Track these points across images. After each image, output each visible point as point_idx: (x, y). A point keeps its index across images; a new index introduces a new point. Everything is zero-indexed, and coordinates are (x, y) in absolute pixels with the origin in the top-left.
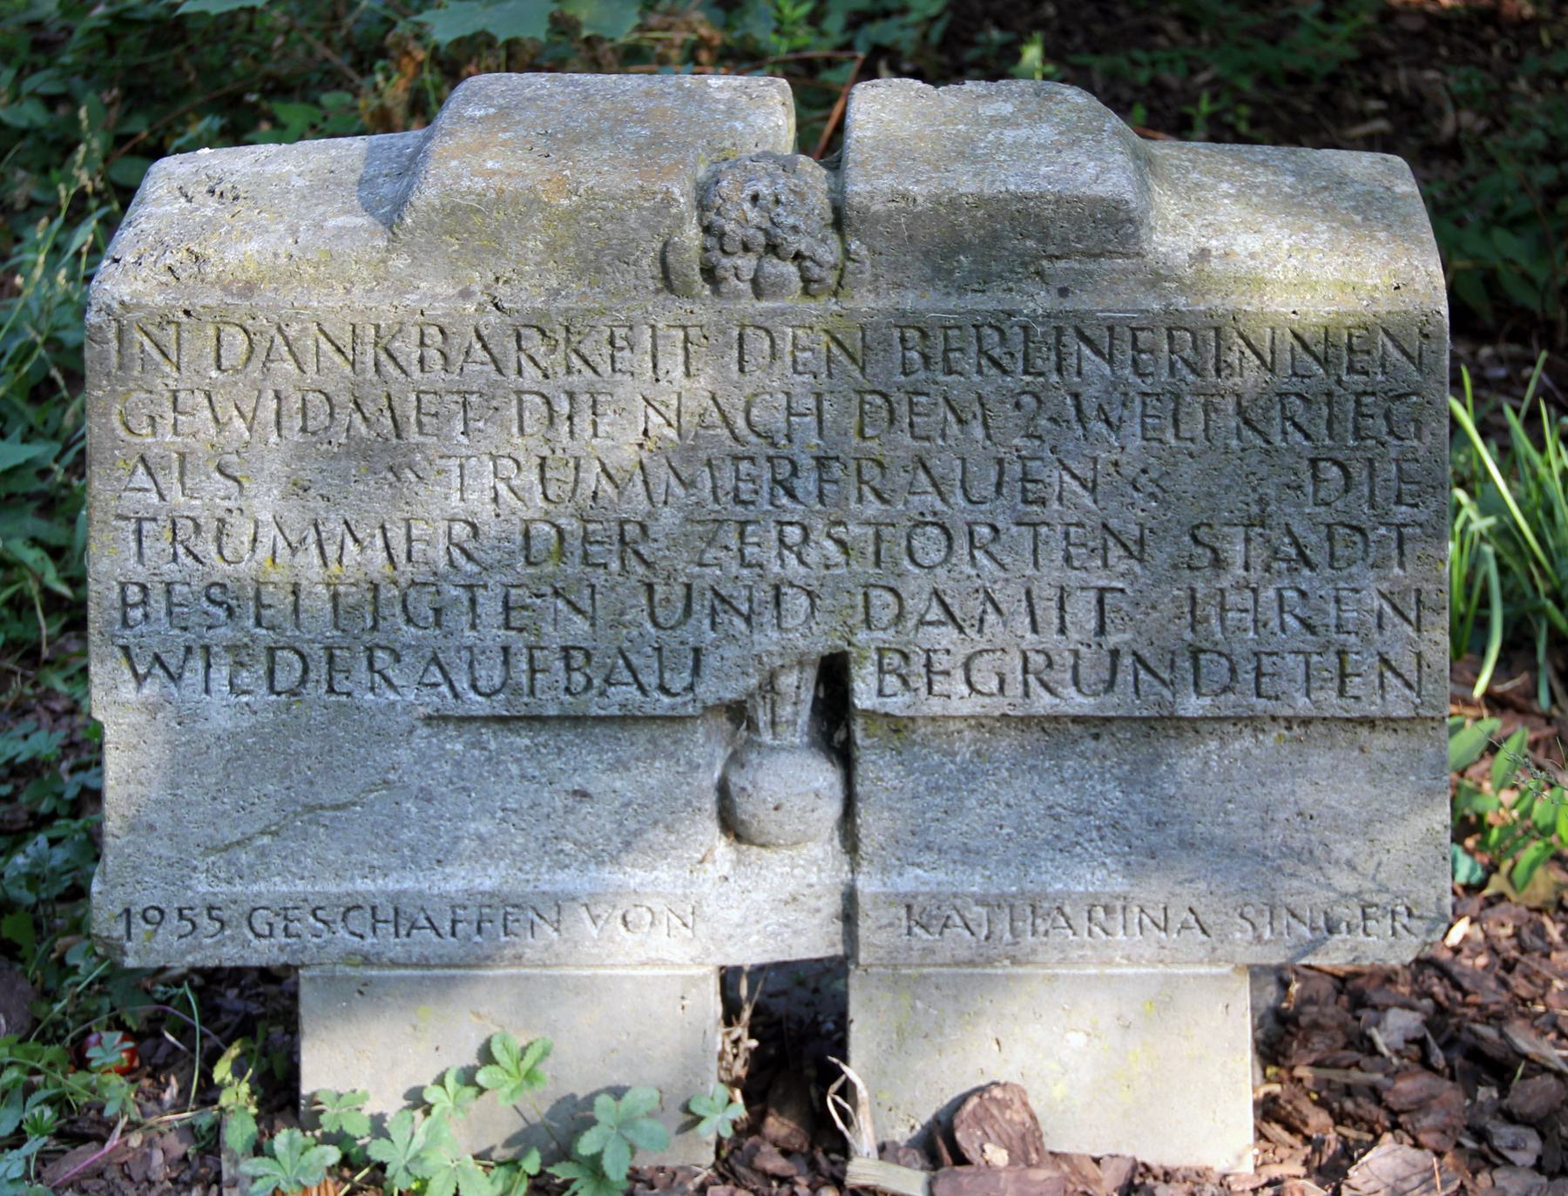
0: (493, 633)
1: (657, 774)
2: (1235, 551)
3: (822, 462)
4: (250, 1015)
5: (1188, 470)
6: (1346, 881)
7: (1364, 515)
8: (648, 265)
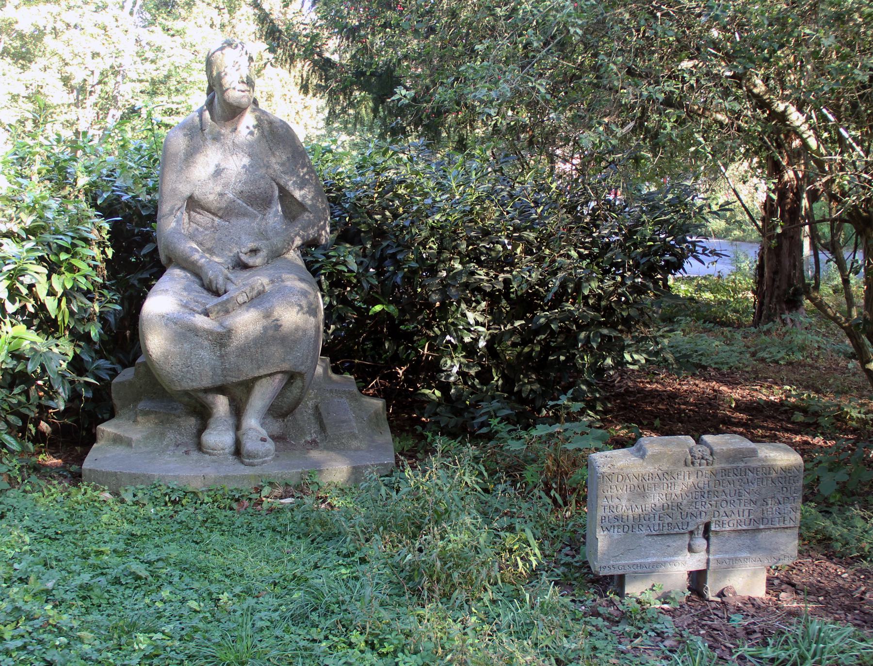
0: (657, 521)
1: (679, 543)
2: (770, 502)
4: (618, 582)
5: (764, 490)
6: (782, 553)
7: (789, 495)
8: (683, 463)
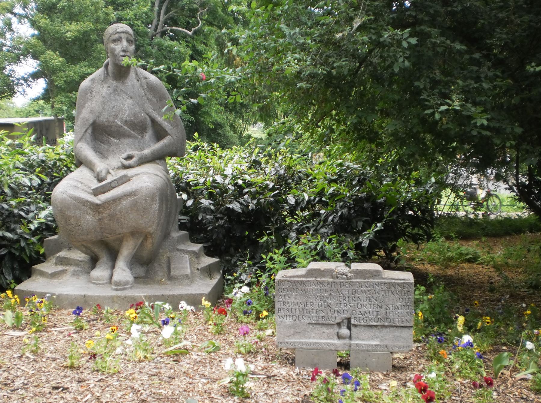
0: (314, 314)
1: (331, 330)
3: (348, 297)
